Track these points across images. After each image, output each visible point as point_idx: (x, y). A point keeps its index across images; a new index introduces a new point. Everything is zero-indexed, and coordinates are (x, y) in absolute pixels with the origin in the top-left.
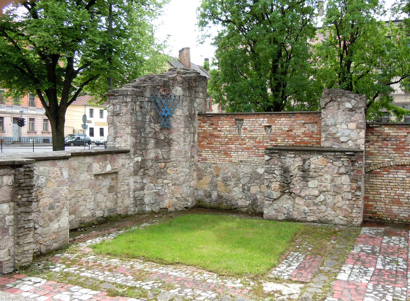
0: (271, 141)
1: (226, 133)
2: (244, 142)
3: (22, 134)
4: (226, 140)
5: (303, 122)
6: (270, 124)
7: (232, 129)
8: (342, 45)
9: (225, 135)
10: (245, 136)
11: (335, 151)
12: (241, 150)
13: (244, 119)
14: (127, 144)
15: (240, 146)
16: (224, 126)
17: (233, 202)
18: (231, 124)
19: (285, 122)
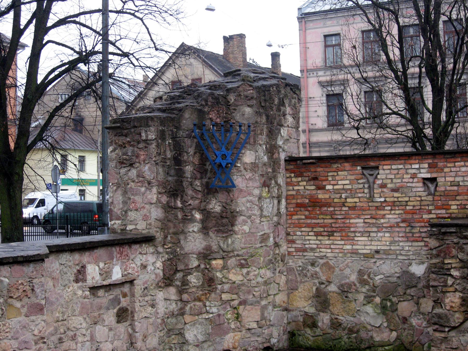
0: (437, 208)
1: (343, 196)
2: (382, 212)
4: (344, 209)
6: (434, 175)
9: (343, 200)
10: (382, 200)
12: (375, 229)
13: (381, 167)
14: (150, 224)
15: (374, 221)
16: (340, 182)
18: (353, 177)
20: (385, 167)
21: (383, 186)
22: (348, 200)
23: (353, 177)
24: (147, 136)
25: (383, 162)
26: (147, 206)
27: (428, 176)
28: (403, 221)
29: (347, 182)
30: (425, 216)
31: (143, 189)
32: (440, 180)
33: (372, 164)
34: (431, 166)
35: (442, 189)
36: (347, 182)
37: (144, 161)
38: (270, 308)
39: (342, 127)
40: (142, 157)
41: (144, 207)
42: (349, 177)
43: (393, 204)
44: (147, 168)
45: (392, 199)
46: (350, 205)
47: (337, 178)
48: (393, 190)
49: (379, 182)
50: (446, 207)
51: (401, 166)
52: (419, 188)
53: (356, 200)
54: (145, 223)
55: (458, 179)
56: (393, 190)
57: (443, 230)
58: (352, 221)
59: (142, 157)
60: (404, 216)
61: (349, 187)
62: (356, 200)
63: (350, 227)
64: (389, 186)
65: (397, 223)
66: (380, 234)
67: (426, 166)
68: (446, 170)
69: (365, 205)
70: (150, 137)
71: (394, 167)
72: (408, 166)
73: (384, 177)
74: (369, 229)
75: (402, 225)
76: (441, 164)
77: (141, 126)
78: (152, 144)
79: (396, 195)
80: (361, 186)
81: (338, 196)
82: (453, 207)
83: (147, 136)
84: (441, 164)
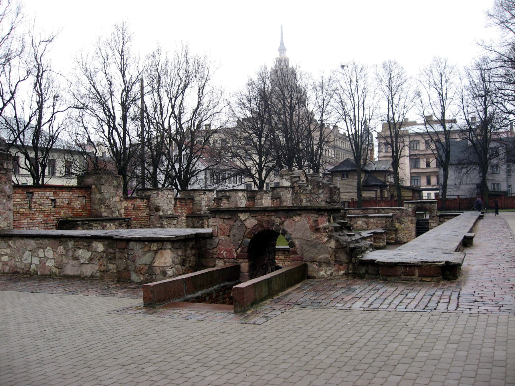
0: (57, 214)
1: (18, 207)
2: (35, 216)
3: (52, 154)
4: (18, 215)
5: (77, 195)
6: (55, 198)
7: (24, 202)
8: (196, 124)
9: (18, 210)
10: (35, 210)
11: (296, 210)
12: (32, 226)
13: (34, 193)
14: (10, 223)
15: (31, 221)
16: (16, 200)
17: (454, 285)
18: (22, 197)
19: (66, 195)
20: (37, 193)
21: (35, 202)
22: (20, 210)
23: (22, 197)
24: (8, 166)
25: (36, 190)
26: (7, 212)
27: (53, 198)
28: (43, 221)
29: (20, 200)
30: (52, 218)
31: (5, 201)
32: (57, 200)
33: (31, 191)
34: (54, 193)
35: (58, 204)
36: (20, 200)
37: (5, 183)
38: (140, 256)
39: (215, 181)
40: (4, 180)
41: (5, 213)
42: (20, 197)
43: (40, 212)
44: (7, 187)
45: (39, 210)
46: (21, 213)
47: (15, 197)
48: (40, 205)
49: (34, 200)
50: (59, 213)
51: (43, 193)
52: (50, 205)
53: (24, 210)
54: (6, 223)
55: (64, 200)
56: (40, 205)
57: (84, 223)
58: (22, 221)
59: (4, 180)
60: (44, 218)
61: (21, 203)
62: (24, 210)
63: (21, 225)
64: (38, 202)
65: (41, 222)
66: (34, 228)
67: (52, 193)
68: (60, 195)
69: (27, 212)
70: (10, 167)
71: (40, 193)
72: (45, 193)
73: (36, 198)
74: (30, 226)
75: (43, 223)
76: (58, 192)
77: (3, 159)
78: (10, 171)
79: (41, 207)
80: (26, 202)
81: (15, 207)
82: (62, 213)
83: (8, 166)
84: (58, 192)
